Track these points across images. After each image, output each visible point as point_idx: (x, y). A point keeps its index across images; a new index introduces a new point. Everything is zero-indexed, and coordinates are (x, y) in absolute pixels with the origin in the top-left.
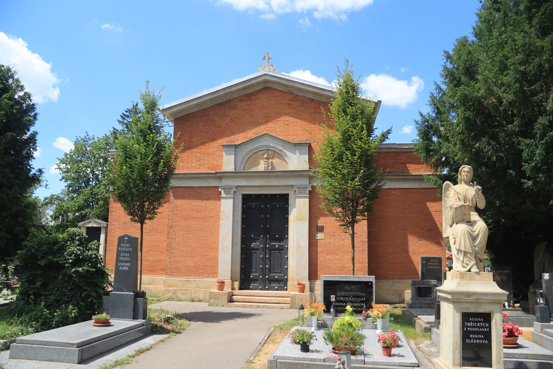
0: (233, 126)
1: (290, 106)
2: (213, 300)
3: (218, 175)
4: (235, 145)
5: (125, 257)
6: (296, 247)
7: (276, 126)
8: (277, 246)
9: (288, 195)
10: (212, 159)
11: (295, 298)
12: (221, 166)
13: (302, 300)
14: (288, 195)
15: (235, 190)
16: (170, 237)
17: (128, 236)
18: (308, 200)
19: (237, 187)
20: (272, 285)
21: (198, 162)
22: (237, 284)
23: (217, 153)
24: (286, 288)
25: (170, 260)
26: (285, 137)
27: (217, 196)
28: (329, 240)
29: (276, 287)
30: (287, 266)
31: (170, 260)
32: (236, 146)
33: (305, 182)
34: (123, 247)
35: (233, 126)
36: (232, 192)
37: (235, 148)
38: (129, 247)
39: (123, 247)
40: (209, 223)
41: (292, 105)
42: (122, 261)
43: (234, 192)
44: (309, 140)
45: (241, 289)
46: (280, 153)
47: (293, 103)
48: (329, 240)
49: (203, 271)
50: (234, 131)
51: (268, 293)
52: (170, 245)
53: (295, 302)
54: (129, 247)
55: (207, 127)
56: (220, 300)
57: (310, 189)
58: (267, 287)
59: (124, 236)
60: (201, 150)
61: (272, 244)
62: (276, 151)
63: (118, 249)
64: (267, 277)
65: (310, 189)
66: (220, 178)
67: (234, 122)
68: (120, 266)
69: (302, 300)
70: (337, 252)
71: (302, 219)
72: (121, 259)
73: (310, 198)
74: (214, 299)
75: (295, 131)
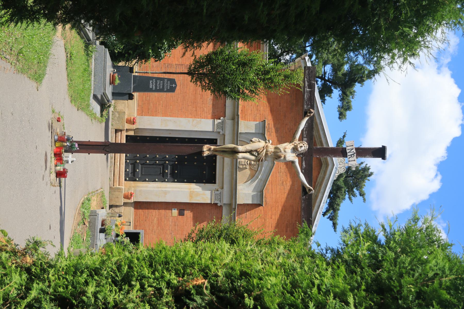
0: (284, 131)
2: (117, 115)
3: (236, 117)
4: (265, 133)
5: (160, 85)
6: (166, 190)
7: (281, 173)
8: (167, 171)
9: (215, 183)
10: (253, 110)
11: (119, 192)
12: (245, 119)
13: (117, 197)
14: (215, 183)
15: (221, 133)
16: (178, 66)
17: (175, 87)
18: (209, 202)
19: (224, 135)
20: (130, 166)
22: (132, 133)
23: (258, 115)
24: (128, 179)
25: (155, 66)
26: (270, 182)
27: (216, 114)
28: (171, 220)
29: (128, 170)
30: (148, 181)
31: (155, 66)
32: (264, 135)
33: (226, 200)
34: (167, 83)
35: (284, 131)
36: (219, 130)
37: (262, 134)
38: (167, 88)
39: (167, 83)
40: (190, 107)
42: (156, 83)
43: (219, 132)
44: (266, 204)
45: (127, 136)
46: (255, 177)
48: (171, 220)
49: (144, 100)
50: (279, 132)
51: (123, 164)
52: (170, 67)
53: (115, 192)
54: (167, 88)
56: (118, 122)
57: (219, 205)
58: (128, 161)
59: (176, 84)
61: (169, 166)
62: (257, 173)
63: (166, 79)
64: (138, 161)
65: (219, 205)
66: (233, 119)
67: (288, 131)
68: (153, 81)
69: (117, 197)
70: (159, 227)
71: (191, 196)
72: (158, 82)
73: (210, 204)
74: (119, 117)
75: (275, 191)
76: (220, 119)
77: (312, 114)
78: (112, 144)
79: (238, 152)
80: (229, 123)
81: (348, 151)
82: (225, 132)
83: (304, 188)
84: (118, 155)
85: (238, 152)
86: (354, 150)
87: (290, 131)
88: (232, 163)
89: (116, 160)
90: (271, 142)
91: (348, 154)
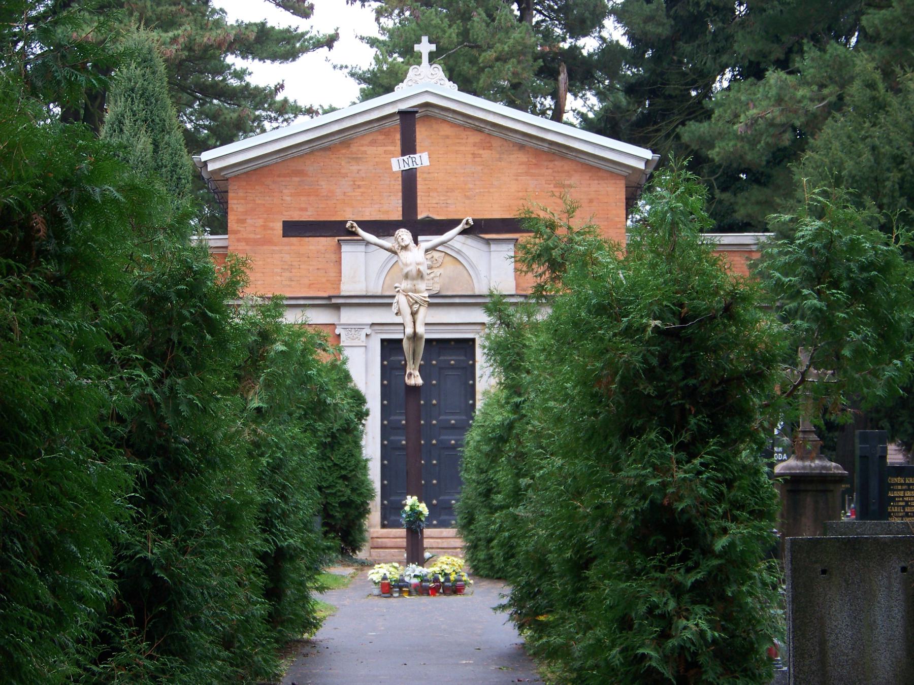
1: (476, 159)
3: (334, 301)
7: (449, 202)
14: (383, 526)
15: (369, 331)
21: (287, 274)
41: (480, 156)
43: (367, 335)
47: (481, 152)
55: (303, 198)
60: (293, 248)
66: (337, 307)
76: (339, 335)
77: (355, 225)
78: (407, 542)
79: (415, 333)
80: (348, 316)
81: (407, 168)
82: (367, 325)
83: (463, 232)
84: (427, 543)
85: (415, 333)
86: (405, 158)
87: (359, 187)
88: (427, 117)
89: (434, 546)
90: (396, 285)
91: (411, 167)
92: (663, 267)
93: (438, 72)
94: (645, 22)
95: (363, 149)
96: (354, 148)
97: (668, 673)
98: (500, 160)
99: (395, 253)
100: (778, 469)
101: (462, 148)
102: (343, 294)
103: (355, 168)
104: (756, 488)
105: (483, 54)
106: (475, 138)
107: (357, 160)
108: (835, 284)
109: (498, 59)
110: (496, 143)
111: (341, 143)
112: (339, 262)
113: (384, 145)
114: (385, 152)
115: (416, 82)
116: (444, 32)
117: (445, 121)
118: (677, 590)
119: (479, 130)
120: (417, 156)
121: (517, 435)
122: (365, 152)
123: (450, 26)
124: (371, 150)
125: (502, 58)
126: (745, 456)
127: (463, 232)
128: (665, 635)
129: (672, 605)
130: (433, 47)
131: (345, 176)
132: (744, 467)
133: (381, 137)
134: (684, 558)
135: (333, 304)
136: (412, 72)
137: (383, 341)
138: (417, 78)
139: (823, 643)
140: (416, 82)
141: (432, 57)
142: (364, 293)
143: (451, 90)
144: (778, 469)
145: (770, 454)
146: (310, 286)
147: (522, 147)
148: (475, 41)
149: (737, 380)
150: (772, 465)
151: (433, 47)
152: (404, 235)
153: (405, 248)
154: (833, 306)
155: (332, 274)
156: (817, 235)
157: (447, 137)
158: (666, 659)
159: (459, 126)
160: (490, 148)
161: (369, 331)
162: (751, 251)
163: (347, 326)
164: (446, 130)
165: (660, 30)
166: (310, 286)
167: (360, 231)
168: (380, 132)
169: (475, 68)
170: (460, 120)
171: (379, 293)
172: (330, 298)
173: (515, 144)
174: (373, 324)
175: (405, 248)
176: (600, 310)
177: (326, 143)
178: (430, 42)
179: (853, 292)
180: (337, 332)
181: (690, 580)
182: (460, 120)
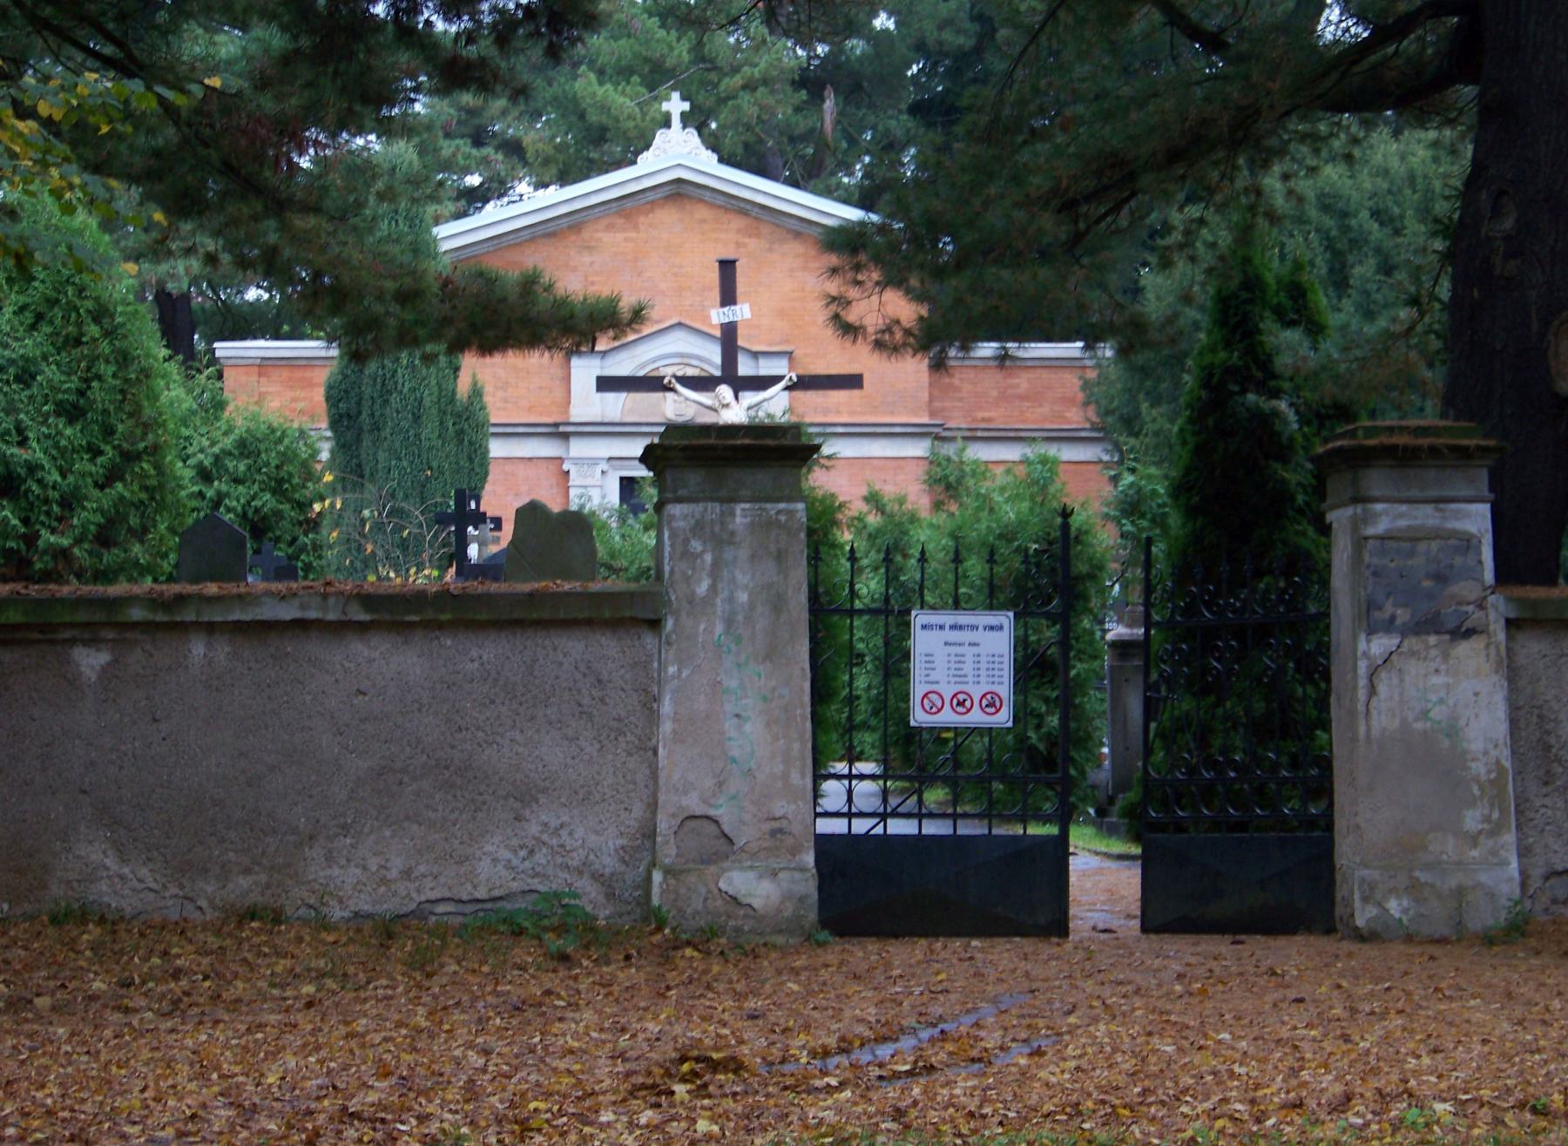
3: (562, 429)
47: (747, 240)
66: (566, 436)
80: (578, 448)
83: (787, 388)
92: (1038, 510)
93: (692, 136)
94: (941, 28)
95: (599, 235)
96: (586, 234)
97: (1041, 747)
98: (770, 250)
99: (716, 410)
100: (1109, 637)
101: (723, 236)
102: (573, 420)
103: (587, 259)
104: (1092, 642)
105: (726, 80)
106: (738, 222)
107: (589, 249)
108: (1142, 516)
109: (744, 87)
110: (765, 229)
111: (570, 227)
112: (567, 379)
113: (624, 230)
114: (626, 239)
115: (665, 151)
116: (671, 48)
117: (701, 201)
118: (1047, 700)
119: (743, 213)
120: (737, 308)
121: (1364, 653)
122: (600, 240)
123: (679, 40)
124: (607, 238)
125: (749, 86)
126: (1086, 623)
127: (787, 388)
128: (1038, 727)
129: (1044, 709)
130: (686, 106)
131: (574, 269)
132: (1084, 629)
133: (620, 221)
134: (1051, 682)
135: (560, 432)
136: (661, 137)
137: (622, 479)
138: (667, 146)
139: (1125, 716)
140: (665, 151)
141: (686, 119)
142: (599, 420)
143: (707, 161)
144: (1109, 637)
145: (1102, 622)
146: (530, 409)
147: (798, 235)
148: (711, 61)
149: (1081, 578)
150: (1105, 631)
151: (686, 106)
152: (725, 391)
153: (727, 406)
154: (1141, 530)
155: (559, 394)
156: (1132, 485)
157: (703, 221)
158: (1040, 739)
159: (720, 207)
160: (758, 235)
161: (604, 466)
162: (1084, 367)
163: (578, 461)
164: (702, 212)
165: (961, 40)
166: (530, 409)
167: (679, 387)
168: (618, 213)
169: (713, 99)
170: (720, 200)
171: (617, 420)
172: (556, 425)
173: (789, 231)
174: (610, 459)
175: (727, 406)
176: (1001, 536)
177: (551, 227)
178: (684, 99)
179: (1153, 521)
180: (565, 467)
181: (1054, 694)
182: (720, 200)
